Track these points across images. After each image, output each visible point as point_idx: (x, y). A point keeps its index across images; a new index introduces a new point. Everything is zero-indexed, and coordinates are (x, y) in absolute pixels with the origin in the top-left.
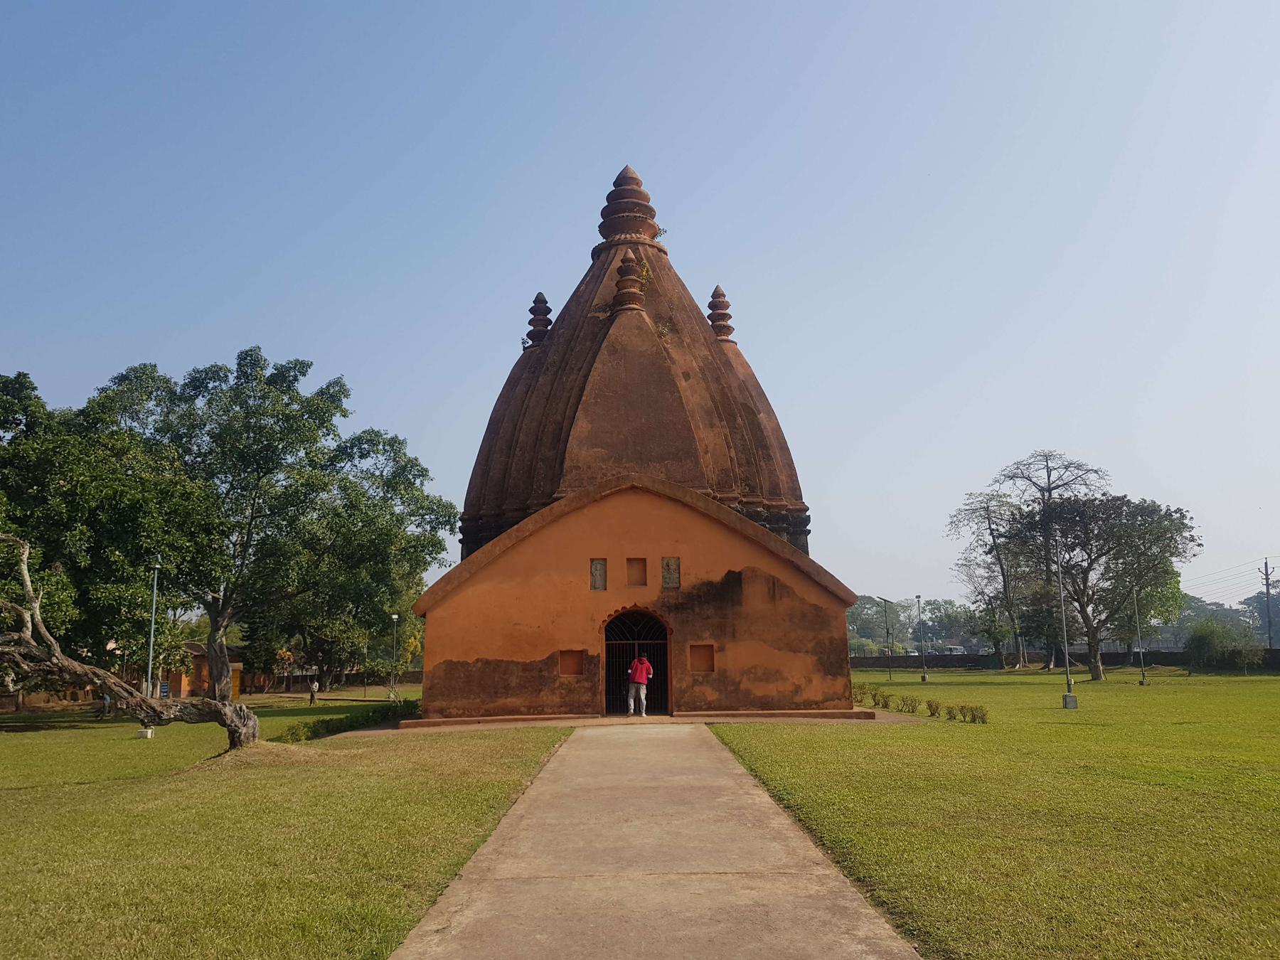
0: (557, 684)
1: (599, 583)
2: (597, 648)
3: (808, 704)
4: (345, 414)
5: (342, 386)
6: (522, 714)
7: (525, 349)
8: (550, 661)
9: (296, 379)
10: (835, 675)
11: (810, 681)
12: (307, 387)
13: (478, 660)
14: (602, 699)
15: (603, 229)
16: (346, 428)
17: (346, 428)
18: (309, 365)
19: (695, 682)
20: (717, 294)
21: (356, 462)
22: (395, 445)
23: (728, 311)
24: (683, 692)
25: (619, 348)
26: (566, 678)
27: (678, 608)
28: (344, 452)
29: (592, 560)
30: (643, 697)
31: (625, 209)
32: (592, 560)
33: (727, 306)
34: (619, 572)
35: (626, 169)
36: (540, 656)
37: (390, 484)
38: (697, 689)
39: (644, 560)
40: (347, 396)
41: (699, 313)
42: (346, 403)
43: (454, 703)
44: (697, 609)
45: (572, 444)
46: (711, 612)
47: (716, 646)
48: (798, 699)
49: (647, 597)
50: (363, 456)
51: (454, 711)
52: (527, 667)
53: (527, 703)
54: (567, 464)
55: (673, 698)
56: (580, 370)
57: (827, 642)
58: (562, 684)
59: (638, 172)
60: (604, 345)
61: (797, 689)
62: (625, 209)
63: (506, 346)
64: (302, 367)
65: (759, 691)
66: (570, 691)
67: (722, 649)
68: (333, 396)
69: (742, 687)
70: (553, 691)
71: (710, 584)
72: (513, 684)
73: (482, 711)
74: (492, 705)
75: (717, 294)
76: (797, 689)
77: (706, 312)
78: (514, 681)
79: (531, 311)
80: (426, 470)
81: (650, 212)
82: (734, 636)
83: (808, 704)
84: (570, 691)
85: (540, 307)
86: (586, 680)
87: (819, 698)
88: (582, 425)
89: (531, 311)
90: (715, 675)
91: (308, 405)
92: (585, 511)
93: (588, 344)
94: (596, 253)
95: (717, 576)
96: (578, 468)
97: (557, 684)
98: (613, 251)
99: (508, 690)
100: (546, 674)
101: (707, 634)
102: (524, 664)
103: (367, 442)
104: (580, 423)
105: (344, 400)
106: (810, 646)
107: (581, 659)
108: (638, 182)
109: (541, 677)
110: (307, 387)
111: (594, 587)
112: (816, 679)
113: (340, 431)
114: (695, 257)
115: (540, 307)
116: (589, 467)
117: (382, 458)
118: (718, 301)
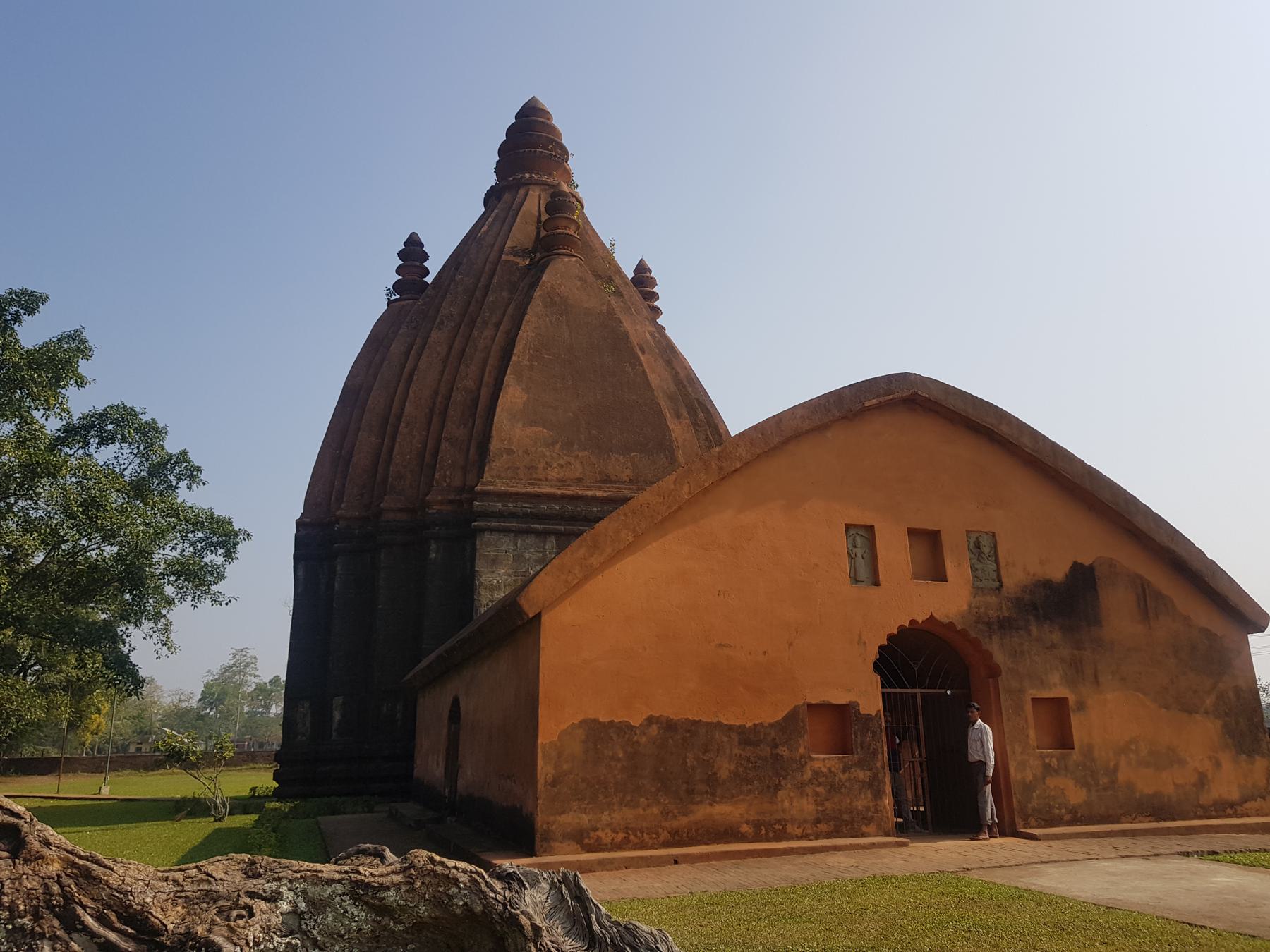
0: (808, 774)
1: (863, 573)
3: (1224, 807)
4: (81, 382)
5: (83, 342)
6: (743, 838)
7: (390, 303)
8: (790, 725)
9: (17, 318)
10: (1251, 753)
11: (1218, 764)
12: (32, 333)
13: (650, 720)
15: (499, 170)
16: (80, 402)
17: (80, 402)
18: (43, 299)
19: (1047, 768)
21: (92, 450)
22: (150, 434)
23: (655, 290)
24: (1028, 788)
25: (557, 299)
26: (824, 762)
27: (1004, 626)
28: (74, 433)
29: (848, 527)
30: (990, 800)
31: (530, 147)
34: (895, 553)
36: (769, 713)
37: (139, 489)
38: (1052, 782)
40: (87, 357)
42: (84, 367)
43: (605, 817)
44: (1034, 630)
45: (501, 417)
46: (1056, 636)
47: (1072, 699)
48: (1205, 799)
49: (949, 601)
50: (104, 441)
51: (606, 836)
52: (748, 737)
53: (753, 816)
54: (495, 445)
56: (498, 325)
57: (1231, 694)
58: (817, 773)
59: (547, 103)
60: (537, 294)
61: (1202, 781)
62: (530, 147)
63: (367, 300)
64: (31, 302)
65: (1147, 783)
66: (833, 788)
67: (1081, 706)
68: (60, 362)
69: (1121, 777)
70: (801, 787)
71: (1047, 584)
72: (724, 774)
73: (664, 835)
74: (684, 820)
76: (1202, 781)
78: (724, 768)
79: (401, 255)
80: (199, 469)
81: (563, 154)
82: (1096, 681)
83: (1224, 807)
84: (833, 788)
85: (413, 252)
86: (860, 764)
87: (1235, 795)
88: (513, 395)
89: (401, 255)
90: (1075, 756)
92: (829, 434)
93: (505, 294)
94: (492, 197)
95: (1058, 572)
96: (510, 452)
97: (808, 774)
98: (522, 192)
99: (713, 787)
100: (783, 751)
101: (1055, 677)
102: (741, 730)
103: (115, 423)
104: (511, 390)
105: (82, 363)
106: (1209, 701)
107: (841, 717)
108: (545, 113)
109: (777, 758)
110: (32, 333)
112: (1226, 758)
113: (70, 405)
114: (622, 212)
115: (413, 252)
116: (527, 452)
117: (126, 450)
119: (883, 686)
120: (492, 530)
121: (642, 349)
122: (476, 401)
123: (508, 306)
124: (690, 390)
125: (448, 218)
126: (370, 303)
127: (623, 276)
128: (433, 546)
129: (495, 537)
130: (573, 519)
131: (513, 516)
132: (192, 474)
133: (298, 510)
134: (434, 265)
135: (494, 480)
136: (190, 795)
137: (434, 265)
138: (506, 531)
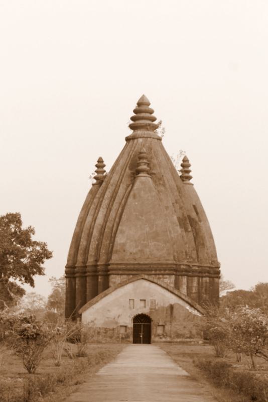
1: (132, 306)
2: (131, 325)
14: (131, 339)
20: (185, 160)
29: (130, 300)
31: (142, 118)
32: (130, 300)
33: (189, 166)
35: (143, 97)
39: (145, 300)
41: (174, 170)
55: (153, 338)
62: (142, 118)
75: (185, 160)
77: (178, 168)
79: (96, 166)
85: (100, 164)
91: (75, 278)
111: (130, 308)
114: (175, 142)
115: (100, 164)
118: (185, 164)
119: (134, 322)
120: (113, 274)
121: (159, 260)
122: (112, 230)
123: (122, 199)
124: (164, 266)
125: (112, 150)
126: (88, 184)
127: (173, 169)
128: (100, 277)
129: (115, 276)
130: (137, 270)
131: (120, 270)
132: (33, 234)
133: (65, 263)
134: (108, 169)
135: (115, 258)
136: (140, 313)
137: (108, 169)
138: (118, 274)
